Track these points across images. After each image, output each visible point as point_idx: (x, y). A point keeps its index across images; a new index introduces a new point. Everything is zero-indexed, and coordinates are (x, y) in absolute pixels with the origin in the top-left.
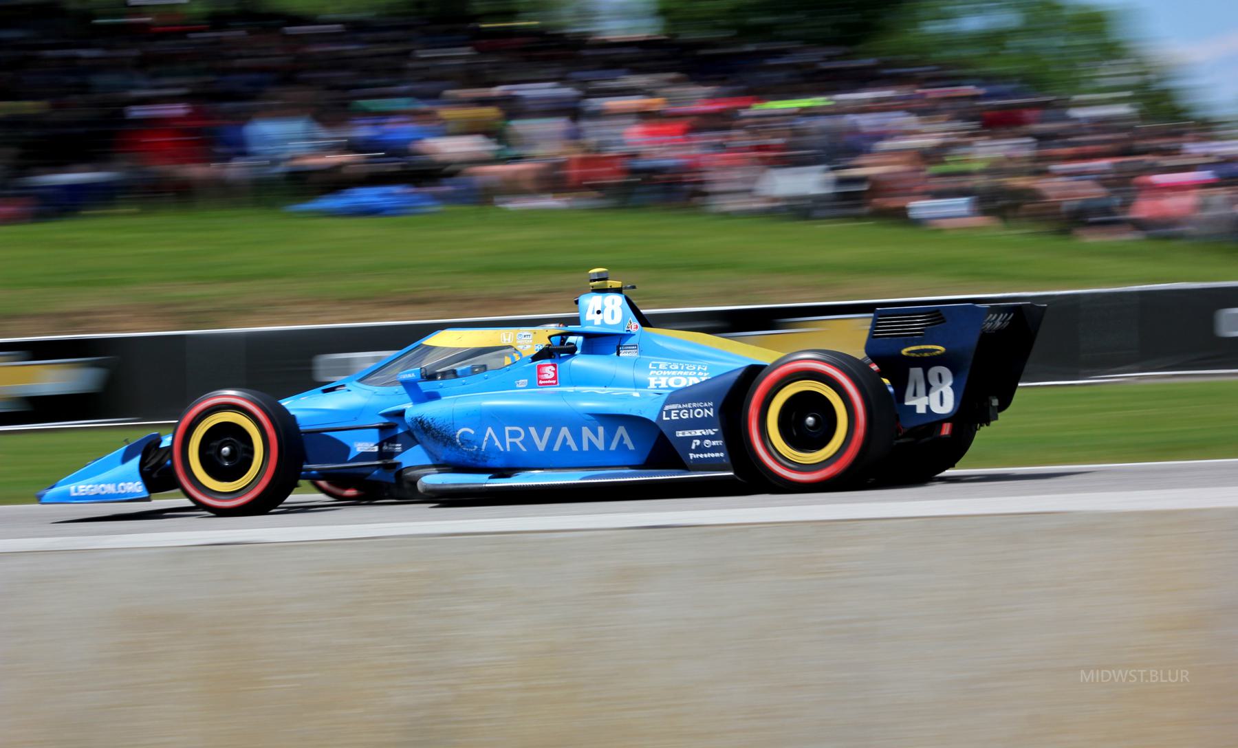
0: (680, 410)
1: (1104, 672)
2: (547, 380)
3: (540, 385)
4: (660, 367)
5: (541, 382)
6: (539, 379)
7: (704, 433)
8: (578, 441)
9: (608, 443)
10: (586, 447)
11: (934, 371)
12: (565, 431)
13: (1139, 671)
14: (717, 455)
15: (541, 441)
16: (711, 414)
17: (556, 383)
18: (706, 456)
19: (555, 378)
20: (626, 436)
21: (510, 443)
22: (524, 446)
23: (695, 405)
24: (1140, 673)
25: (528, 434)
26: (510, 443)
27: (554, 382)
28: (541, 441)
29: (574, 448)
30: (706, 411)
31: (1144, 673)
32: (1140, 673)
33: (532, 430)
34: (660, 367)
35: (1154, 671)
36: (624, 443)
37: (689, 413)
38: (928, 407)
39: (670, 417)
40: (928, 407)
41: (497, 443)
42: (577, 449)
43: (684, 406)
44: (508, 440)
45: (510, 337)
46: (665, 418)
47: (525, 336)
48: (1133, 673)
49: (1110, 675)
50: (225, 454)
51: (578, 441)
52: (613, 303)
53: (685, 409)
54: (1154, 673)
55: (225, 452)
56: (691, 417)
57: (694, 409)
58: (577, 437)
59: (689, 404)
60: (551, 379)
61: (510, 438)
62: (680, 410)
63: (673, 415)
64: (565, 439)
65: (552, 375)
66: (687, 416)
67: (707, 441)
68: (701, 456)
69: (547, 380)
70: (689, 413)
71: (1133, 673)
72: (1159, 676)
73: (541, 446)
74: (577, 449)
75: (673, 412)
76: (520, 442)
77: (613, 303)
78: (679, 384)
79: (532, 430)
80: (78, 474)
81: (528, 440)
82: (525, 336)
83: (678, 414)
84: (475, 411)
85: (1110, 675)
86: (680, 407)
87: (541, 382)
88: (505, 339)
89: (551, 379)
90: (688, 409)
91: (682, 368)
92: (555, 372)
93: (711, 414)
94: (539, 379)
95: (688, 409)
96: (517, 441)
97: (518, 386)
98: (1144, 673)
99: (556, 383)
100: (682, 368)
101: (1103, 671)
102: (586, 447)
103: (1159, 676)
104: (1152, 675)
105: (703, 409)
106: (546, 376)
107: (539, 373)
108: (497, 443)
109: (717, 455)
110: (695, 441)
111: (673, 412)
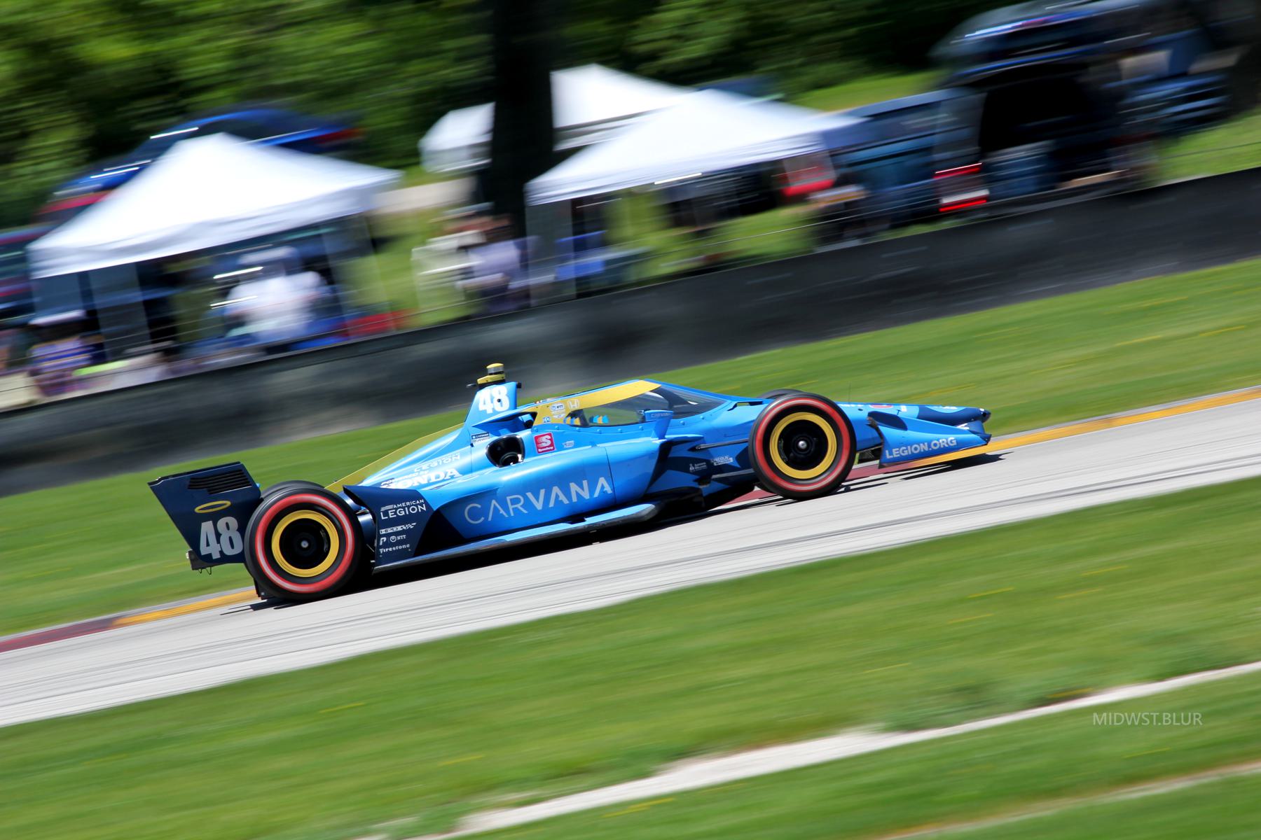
0: (396, 509)
1: (1117, 716)
2: (545, 447)
3: (539, 452)
4: (423, 468)
5: (540, 450)
6: (538, 448)
7: (405, 528)
8: (568, 495)
9: (592, 491)
10: (575, 499)
11: (221, 523)
12: (556, 490)
13: (1152, 714)
14: (404, 546)
15: (538, 501)
16: (424, 509)
17: (553, 449)
18: (394, 549)
19: (552, 445)
20: (560, 494)
21: (513, 509)
22: (525, 509)
23: (408, 504)
24: (1153, 716)
25: (526, 498)
26: (513, 509)
27: (552, 448)
28: (538, 501)
29: (566, 501)
30: (419, 507)
31: (1157, 716)
32: (1153, 716)
33: (529, 495)
34: (423, 468)
35: (1164, 716)
36: (560, 499)
37: (405, 510)
38: (221, 552)
39: (388, 516)
40: (221, 552)
41: (502, 512)
42: (568, 502)
43: (398, 505)
44: (511, 507)
45: (576, 403)
46: (383, 518)
47: (558, 407)
48: (1145, 716)
49: (1123, 717)
50: (805, 446)
51: (568, 495)
52: (500, 393)
53: (400, 507)
54: (1167, 716)
55: (803, 445)
56: (407, 513)
57: (409, 507)
58: (567, 493)
59: (403, 504)
60: (548, 447)
61: (512, 504)
62: (396, 509)
63: (390, 514)
64: (557, 496)
65: (549, 443)
66: (403, 513)
67: (393, 537)
68: (390, 549)
69: (545, 447)
70: (405, 510)
71: (1145, 716)
72: (1172, 718)
73: (539, 506)
74: (568, 502)
75: (390, 512)
76: (522, 506)
77: (500, 393)
78: (438, 478)
79: (529, 495)
80: (91, 616)
81: (528, 504)
82: (558, 407)
83: (395, 513)
84: (441, 494)
85: (1123, 717)
86: (395, 506)
87: (540, 450)
88: (572, 406)
89: (548, 447)
90: (404, 508)
91: (440, 463)
92: (551, 440)
93: (424, 509)
94: (538, 448)
95: (404, 508)
96: (519, 506)
97: (565, 446)
98: (1157, 716)
99: (553, 449)
100: (440, 463)
101: (1115, 714)
102: (575, 499)
103: (1172, 718)
104: (1164, 719)
105: (416, 505)
106: (544, 445)
107: (537, 443)
108: (502, 512)
109: (404, 546)
110: (382, 539)
111: (390, 512)
